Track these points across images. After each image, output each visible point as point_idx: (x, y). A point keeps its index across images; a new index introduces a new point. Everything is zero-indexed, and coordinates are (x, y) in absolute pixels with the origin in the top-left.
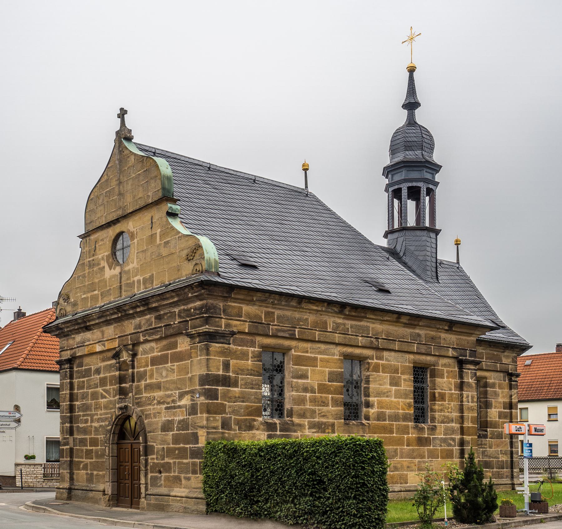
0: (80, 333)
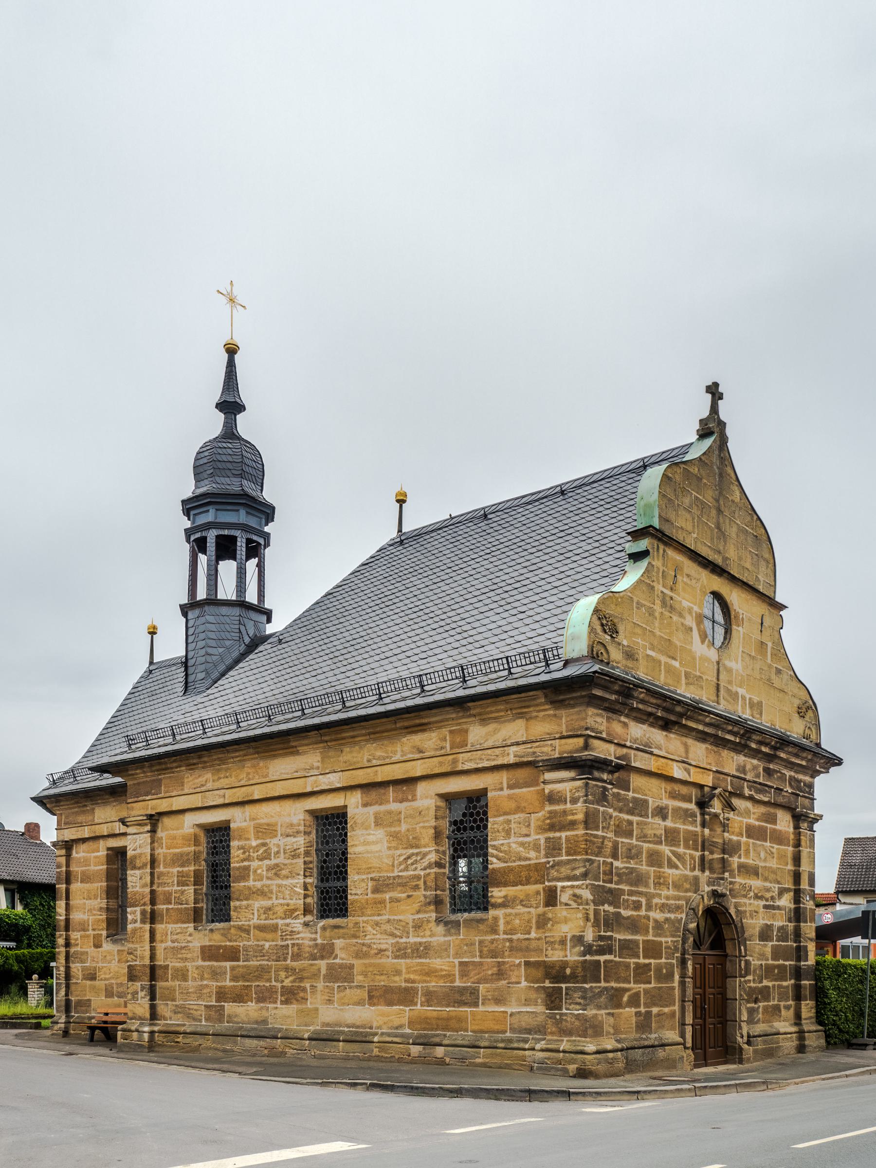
0: (642, 721)
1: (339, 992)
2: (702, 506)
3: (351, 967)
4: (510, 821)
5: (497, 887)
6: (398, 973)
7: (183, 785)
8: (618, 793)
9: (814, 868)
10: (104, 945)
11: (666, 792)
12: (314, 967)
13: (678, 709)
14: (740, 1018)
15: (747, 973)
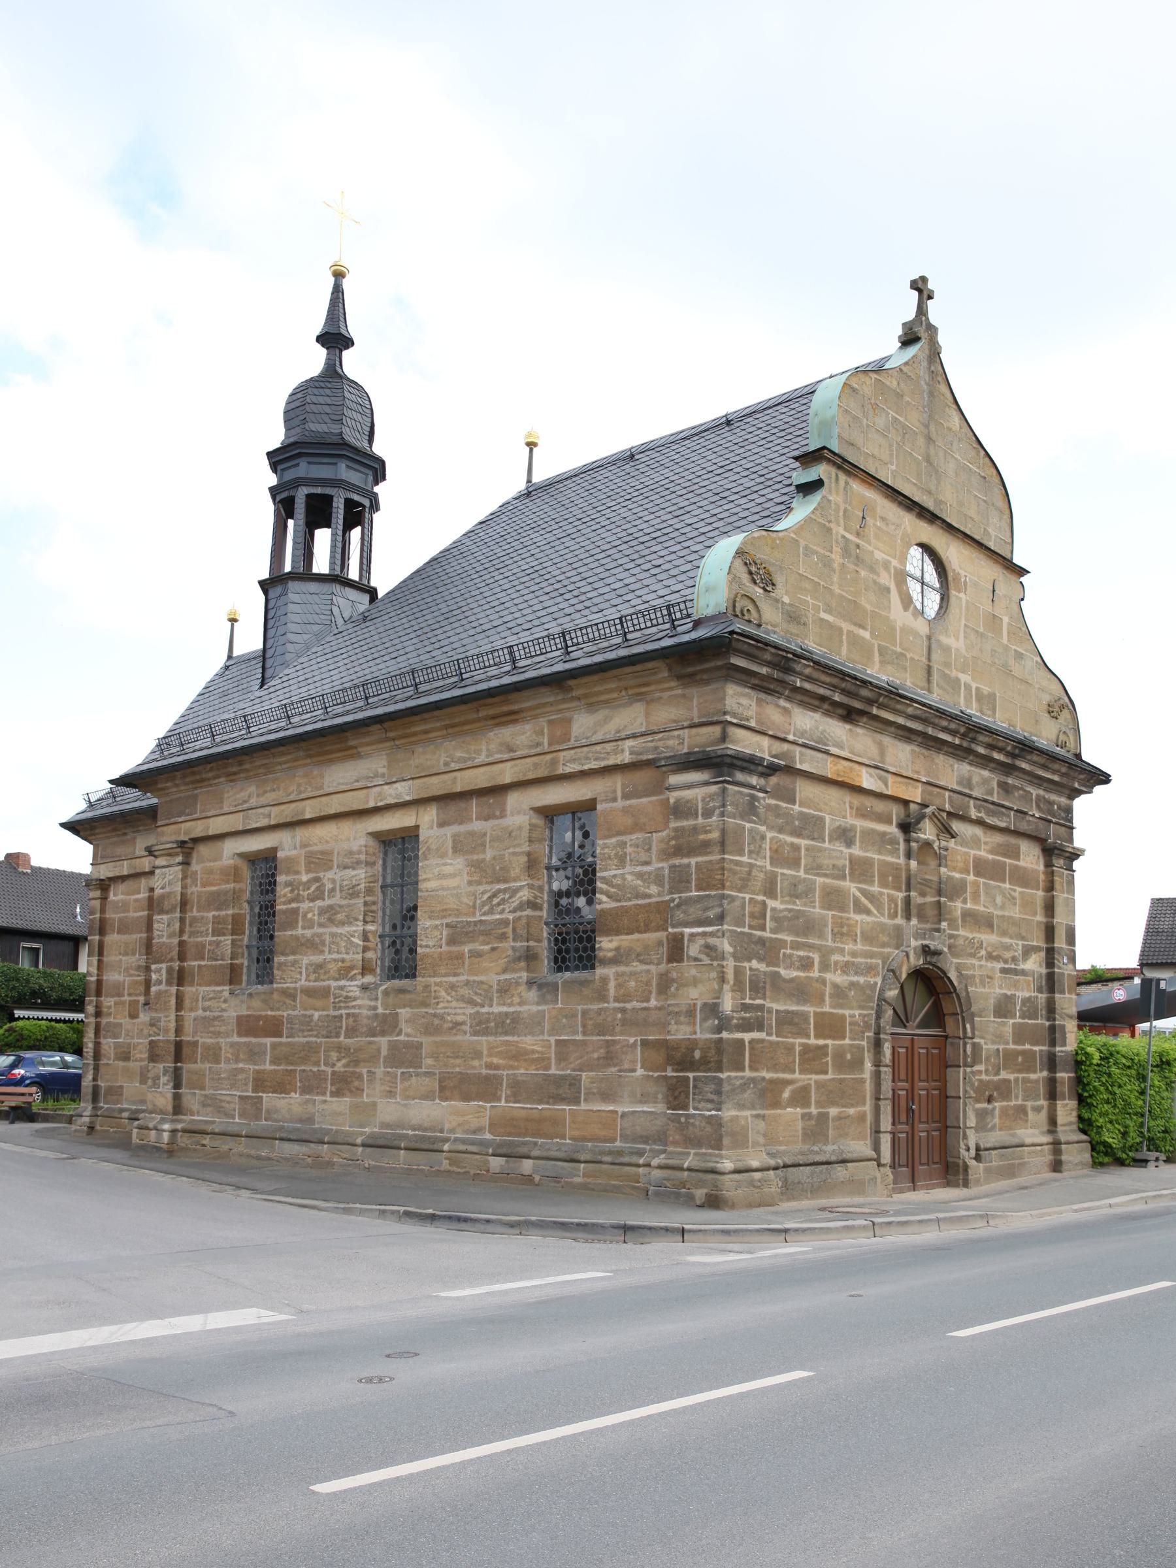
0: (814, 709)
1: (402, 1080)
2: (905, 431)
3: (419, 1046)
4: (625, 843)
5: (607, 935)
6: (478, 1055)
7: (222, 802)
8: (777, 806)
9: (1074, 921)
10: (141, 1015)
11: (851, 808)
12: (374, 1046)
13: (865, 692)
14: (965, 1123)
15: (976, 1059)
